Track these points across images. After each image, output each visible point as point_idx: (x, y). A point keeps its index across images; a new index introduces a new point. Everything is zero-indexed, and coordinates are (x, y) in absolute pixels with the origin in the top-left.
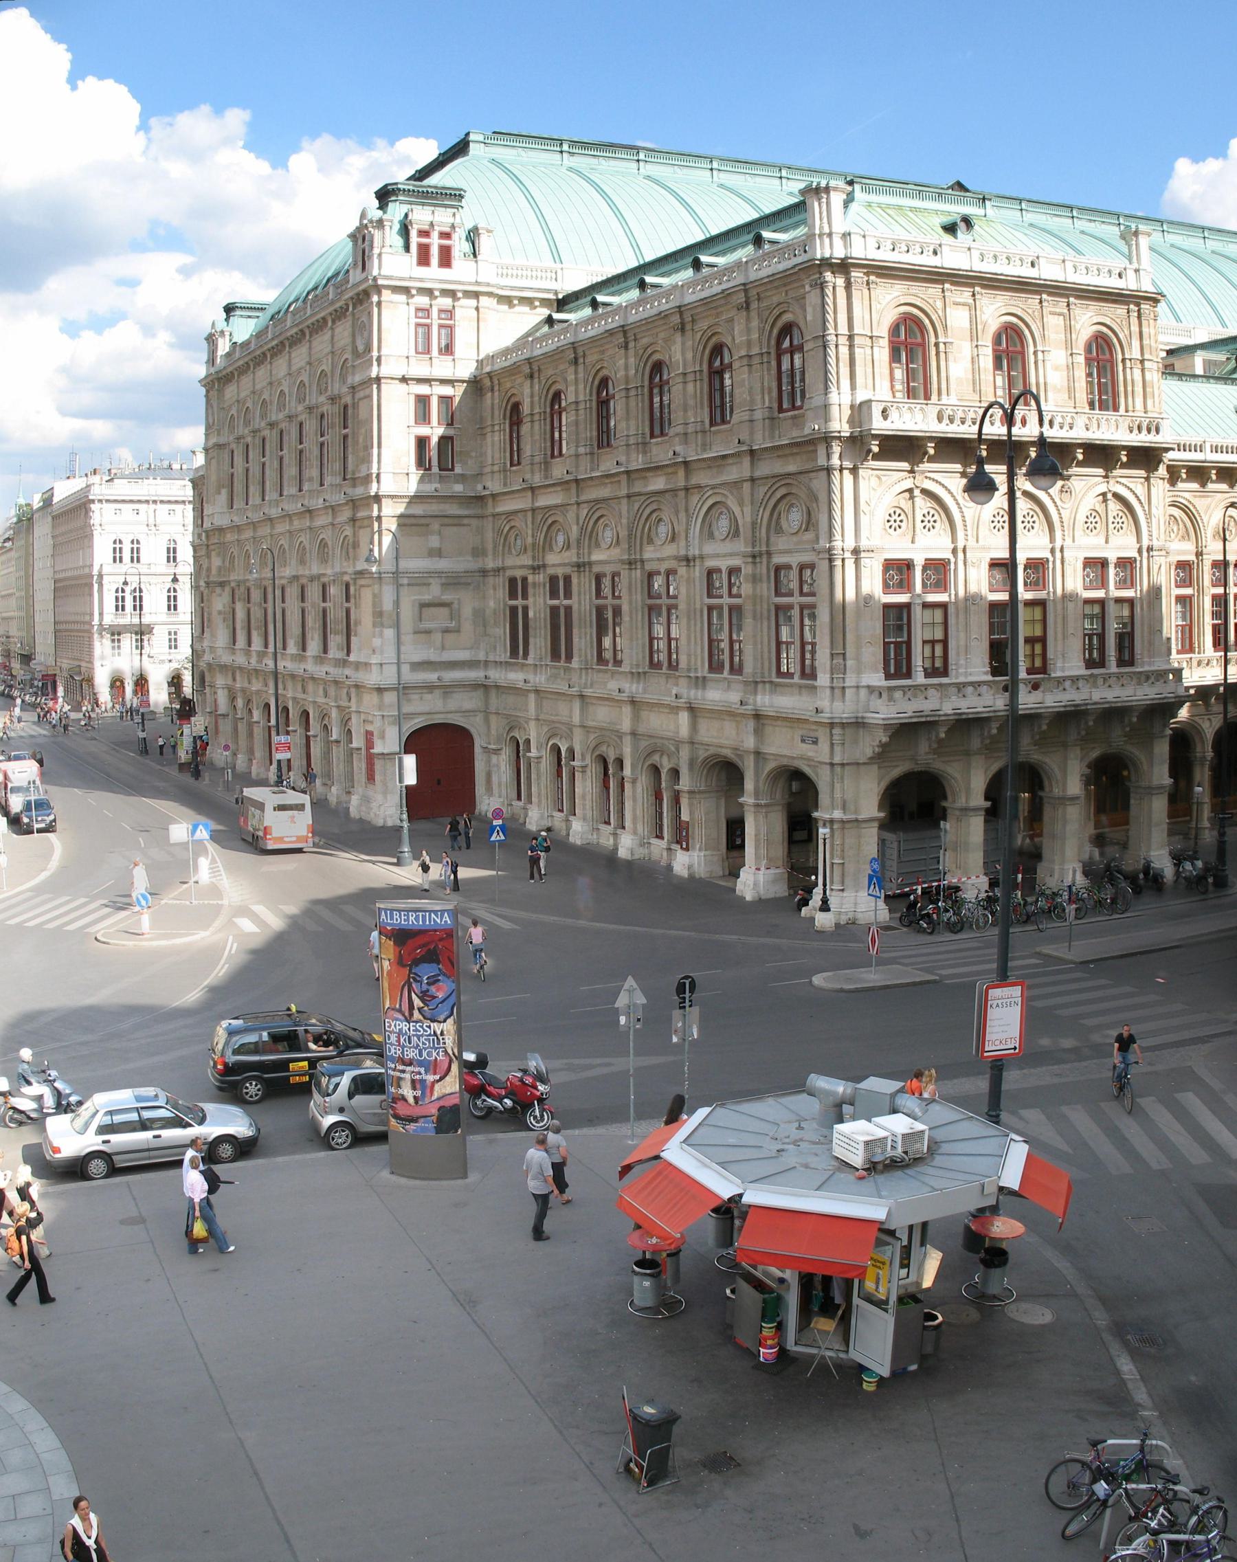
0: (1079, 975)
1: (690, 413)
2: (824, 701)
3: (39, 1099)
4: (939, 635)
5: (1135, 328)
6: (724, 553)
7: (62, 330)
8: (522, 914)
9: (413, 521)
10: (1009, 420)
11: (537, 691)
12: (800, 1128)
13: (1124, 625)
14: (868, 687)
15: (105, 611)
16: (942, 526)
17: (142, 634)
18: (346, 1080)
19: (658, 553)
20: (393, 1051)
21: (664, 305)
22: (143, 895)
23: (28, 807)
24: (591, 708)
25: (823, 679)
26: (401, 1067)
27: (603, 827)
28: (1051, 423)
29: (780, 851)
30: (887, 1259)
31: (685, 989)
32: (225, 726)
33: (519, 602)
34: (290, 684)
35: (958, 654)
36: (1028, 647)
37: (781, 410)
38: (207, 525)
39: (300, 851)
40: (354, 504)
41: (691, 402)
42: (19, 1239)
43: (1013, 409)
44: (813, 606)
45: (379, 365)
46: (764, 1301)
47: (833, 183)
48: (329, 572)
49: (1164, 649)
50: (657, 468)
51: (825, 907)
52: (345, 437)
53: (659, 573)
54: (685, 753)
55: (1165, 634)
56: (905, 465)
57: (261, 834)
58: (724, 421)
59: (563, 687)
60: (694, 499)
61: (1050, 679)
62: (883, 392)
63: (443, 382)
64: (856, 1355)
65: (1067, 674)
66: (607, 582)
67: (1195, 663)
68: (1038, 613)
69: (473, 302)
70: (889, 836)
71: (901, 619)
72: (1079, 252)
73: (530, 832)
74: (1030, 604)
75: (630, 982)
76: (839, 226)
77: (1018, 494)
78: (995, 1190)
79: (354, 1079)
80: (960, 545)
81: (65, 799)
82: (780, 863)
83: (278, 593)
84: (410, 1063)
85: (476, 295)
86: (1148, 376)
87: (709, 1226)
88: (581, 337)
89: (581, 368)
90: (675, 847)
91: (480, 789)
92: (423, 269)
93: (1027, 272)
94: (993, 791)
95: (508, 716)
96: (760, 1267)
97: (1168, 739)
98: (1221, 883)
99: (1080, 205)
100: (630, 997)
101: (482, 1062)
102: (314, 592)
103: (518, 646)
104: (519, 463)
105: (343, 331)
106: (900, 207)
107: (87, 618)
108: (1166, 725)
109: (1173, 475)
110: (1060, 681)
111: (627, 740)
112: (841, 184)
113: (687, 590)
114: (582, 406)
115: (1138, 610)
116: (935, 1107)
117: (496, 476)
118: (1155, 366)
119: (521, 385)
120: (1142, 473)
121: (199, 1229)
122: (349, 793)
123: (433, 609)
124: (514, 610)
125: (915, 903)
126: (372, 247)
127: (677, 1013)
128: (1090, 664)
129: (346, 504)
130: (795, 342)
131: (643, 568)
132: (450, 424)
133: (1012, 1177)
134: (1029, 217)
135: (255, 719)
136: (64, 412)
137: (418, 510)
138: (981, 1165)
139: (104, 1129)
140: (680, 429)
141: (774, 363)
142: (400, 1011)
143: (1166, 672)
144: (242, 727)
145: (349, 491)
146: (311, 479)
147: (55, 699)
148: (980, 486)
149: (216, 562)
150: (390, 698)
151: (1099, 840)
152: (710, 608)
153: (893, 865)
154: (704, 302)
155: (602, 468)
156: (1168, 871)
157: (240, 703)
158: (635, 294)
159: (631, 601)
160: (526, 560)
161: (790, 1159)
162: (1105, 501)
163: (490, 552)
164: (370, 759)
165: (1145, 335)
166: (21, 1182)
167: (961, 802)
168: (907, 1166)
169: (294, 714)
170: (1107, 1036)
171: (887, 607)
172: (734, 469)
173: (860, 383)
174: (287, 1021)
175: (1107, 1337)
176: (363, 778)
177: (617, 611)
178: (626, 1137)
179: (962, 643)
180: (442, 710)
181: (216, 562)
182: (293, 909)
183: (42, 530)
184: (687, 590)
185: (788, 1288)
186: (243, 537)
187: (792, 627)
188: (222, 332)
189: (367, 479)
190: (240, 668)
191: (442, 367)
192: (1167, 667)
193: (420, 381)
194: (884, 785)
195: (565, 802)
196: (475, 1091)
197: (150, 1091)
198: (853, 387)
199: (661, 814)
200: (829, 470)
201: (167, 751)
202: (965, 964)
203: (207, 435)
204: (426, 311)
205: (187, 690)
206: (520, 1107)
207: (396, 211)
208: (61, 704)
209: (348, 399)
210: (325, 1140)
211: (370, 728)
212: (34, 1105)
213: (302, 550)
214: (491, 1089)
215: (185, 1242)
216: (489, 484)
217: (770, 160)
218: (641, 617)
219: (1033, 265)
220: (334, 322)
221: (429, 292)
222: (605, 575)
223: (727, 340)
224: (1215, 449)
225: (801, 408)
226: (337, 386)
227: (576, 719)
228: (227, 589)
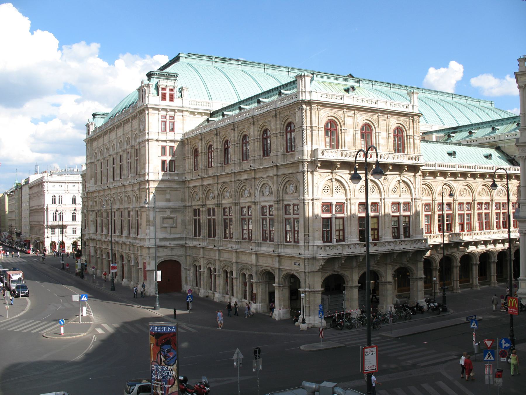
1: (256, 153)
4: (341, 228)
5: (411, 125)
6: (267, 201)
7: (31, 122)
9: (161, 189)
10: (366, 155)
11: (203, 248)
13: (406, 224)
14: (317, 246)
15: (49, 220)
16: (342, 191)
17: (63, 229)
18: (136, 388)
19: (245, 200)
21: (247, 115)
23: (18, 287)
25: (301, 243)
26: (157, 383)
27: (226, 296)
28: (381, 157)
29: (287, 303)
31: (257, 352)
32: (93, 260)
33: (197, 217)
34: (117, 246)
35: (348, 234)
36: (372, 232)
37: (287, 152)
38: (87, 190)
40: (140, 183)
41: (256, 149)
43: (367, 152)
44: (298, 218)
45: (148, 135)
47: (306, 74)
48: (131, 207)
49: (421, 232)
50: (245, 171)
51: (304, 322)
52: (137, 160)
53: (245, 207)
54: (254, 269)
55: (421, 227)
56: (330, 171)
58: (267, 156)
59: (213, 247)
60: (258, 182)
61: (380, 242)
62: (322, 146)
63: (171, 141)
65: (386, 240)
66: (227, 210)
67: (432, 237)
68: (376, 220)
69: (181, 114)
70: (325, 297)
72: (392, 99)
74: (372, 217)
75: (238, 350)
76: (308, 89)
77: (369, 181)
79: (140, 387)
80: (348, 198)
81: (33, 285)
83: (113, 214)
84: (160, 381)
85: (182, 111)
86: (415, 141)
88: (219, 126)
89: (219, 137)
91: (183, 283)
92: (164, 102)
93: (373, 106)
94: (362, 280)
95: (193, 257)
97: (423, 263)
98: (445, 310)
99: (394, 83)
100: (238, 355)
101: (185, 380)
102: (125, 214)
103: (197, 233)
104: (197, 170)
105: (135, 123)
106: (330, 83)
107: (42, 223)
108: (422, 257)
109: (424, 174)
110: (384, 243)
111: (234, 265)
112: (309, 74)
113: (255, 213)
114: (219, 150)
115: (411, 219)
117: (189, 174)
118: (418, 138)
119: (198, 143)
120: (413, 174)
124: (195, 220)
126: (145, 94)
127: (254, 361)
128: (394, 237)
129: (137, 183)
130: (292, 129)
132: (173, 156)
134: (375, 87)
135: (132, 264)
136: (33, 151)
137: (162, 185)
140: (252, 158)
141: (285, 136)
142: (157, 362)
143: (422, 240)
145: (138, 179)
147: (29, 248)
148: (355, 178)
149: (90, 203)
150: (152, 251)
152: (263, 219)
154: (261, 114)
155: (226, 171)
156: (425, 305)
157: (98, 252)
158: (237, 111)
159: (235, 217)
162: (399, 183)
163: (187, 200)
164: (145, 272)
165: (415, 128)
167: (350, 284)
169: (118, 256)
171: (323, 218)
172: (271, 172)
173: (314, 143)
177: (231, 220)
179: (349, 230)
180: (170, 254)
181: (90, 203)
182: (116, 325)
183: (25, 191)
184: (255, 213)
187: (291, 226)
188: (92, 123)
189: (144, 175)
191: (170, 136)
192: (422, 238)
193: (163, 141)
194: (323, 279)
195: (213, 287)
198: (312, 144)
199: (246, 291)
200: (303, 172)
203: (87, 159)
204: (165, 117)
205: (79, 248)
207: (154, 81)
209: (137, 147)
211: (145, 261)
213: (121, 199)
214: (189, 390)
216: (187, 177)
217: (285, 66)
219: (376, 103)
220: (132, 120)
221: (166, 110)
222: (227, 208)
223: (269, 128)
224: (460, 167)
225: (294, 151)
226: (133, 142)
227: (217, 258)
228: (94, 213)
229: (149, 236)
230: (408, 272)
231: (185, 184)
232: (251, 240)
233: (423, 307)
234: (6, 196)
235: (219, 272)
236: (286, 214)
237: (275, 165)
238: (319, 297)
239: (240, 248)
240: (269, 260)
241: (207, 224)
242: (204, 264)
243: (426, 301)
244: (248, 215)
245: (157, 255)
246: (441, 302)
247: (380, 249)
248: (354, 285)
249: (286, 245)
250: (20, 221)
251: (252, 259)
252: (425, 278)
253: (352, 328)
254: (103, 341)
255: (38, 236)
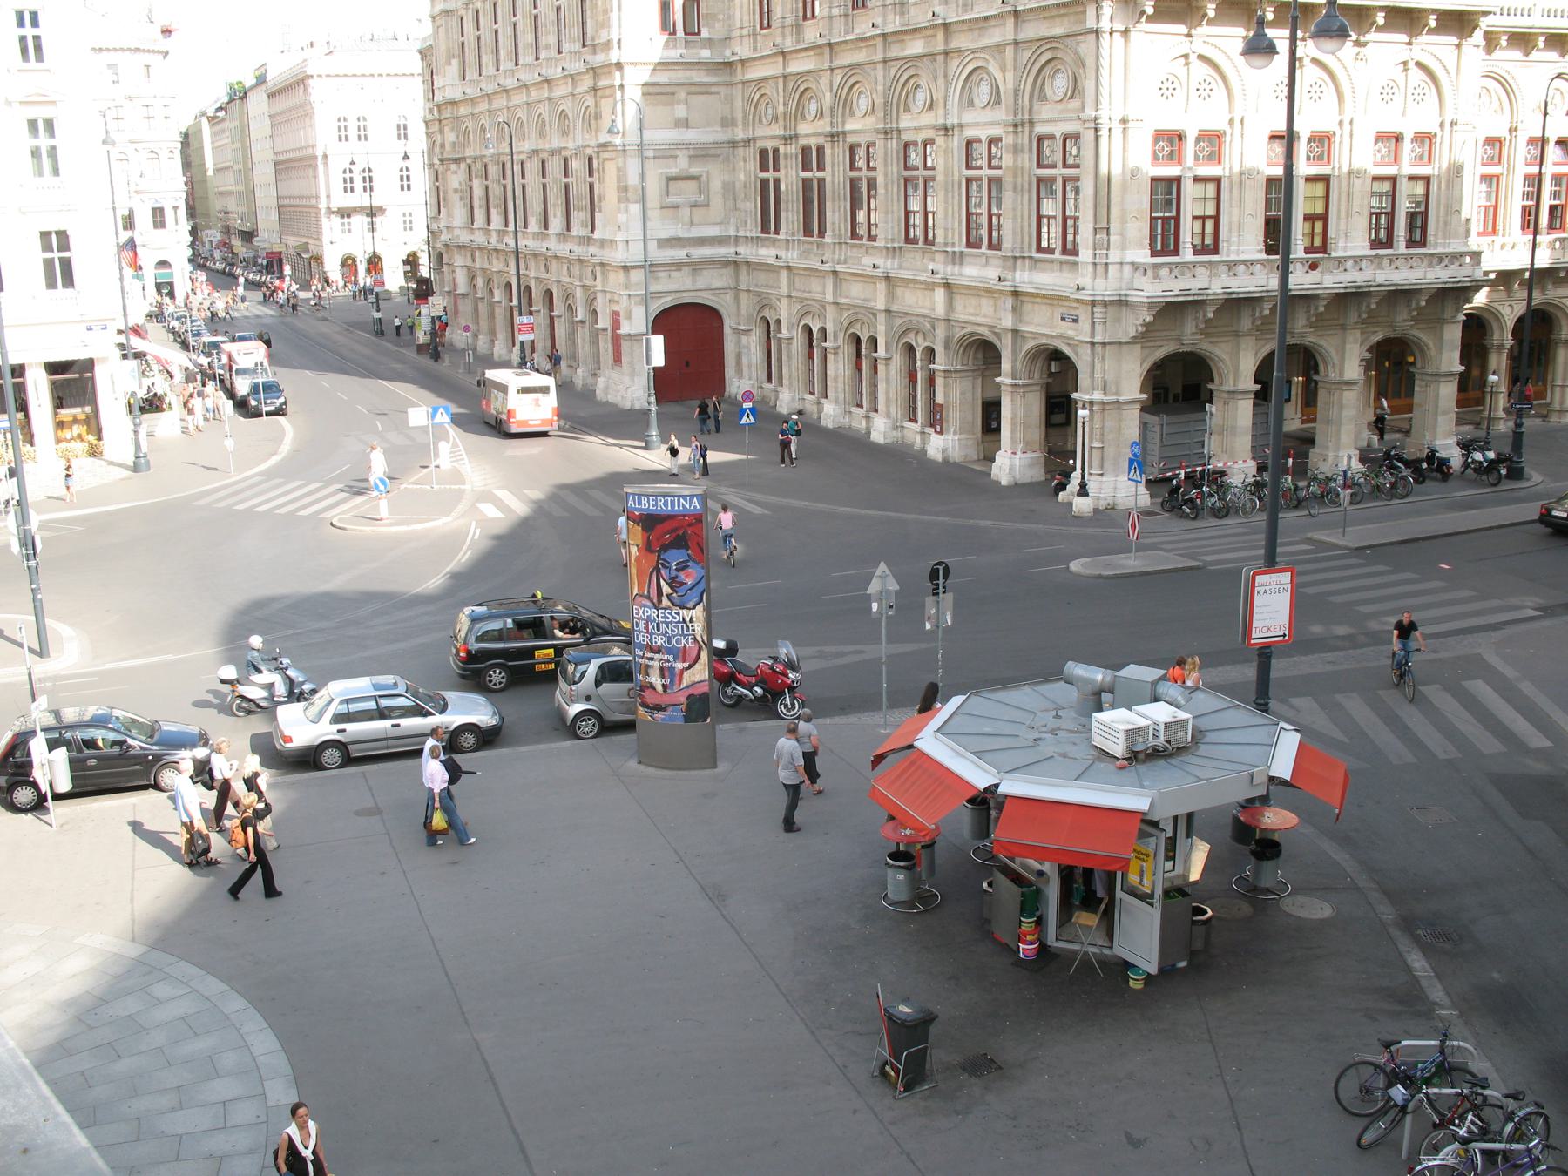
0: (1354, 561)
2: (1085, 278)
3: (270, 687)
6: (984, 122)
8: (773, 499)
9: (658, 89)
11: (788, 268)
12: (1057, 716)
13: (1418, 204)
14: (1133, 264)
18: (592, 668)
20: (641, 638)
22: (382, 481)
23: (255, 389)
24: (845, 285)
25: (1085, 255)
27: (855, 410)
29: (1037, 433)
30: (1150, 850)
31: (938, 575)
32: (465, 307)
33: (770, 175)
34: (532, 264)
35: (1230, 230)
38: (438, 98)
39: (544, 434)
40: (594, 71)
42: (245, 831)
44: (1077, 179)
46: (1023, 895)
48: (570, 145)
49: (1462, 230)
50: (915, 30)
51: (1083, 491)
54: (940, 333)
55: (1464, 216)
56: (1182, 29)
57: (504, 417)
59: (818, 265)
60: (955, 63)
61: (1330, 259)
64: (1121, 950)
66: (861, 152)
68: (1320, 187)
71: (1170, 193)
73: (780, 415)
74: (1309, 179)
75: (882, 568)
78: (1265, 779)
79: (601, 667)
81: (296, 383)
82: (1037, 447)
83: (517, 168)
87: (963, 818)
90: (930, 430)
95: (758, 294)
96: (1018, 860)
98: (1516, 474)
100: (882, 582)
101: (731, 650)
102: (555, 167)
103: (769, 222)
107: (313, 202)
108: (1458, 309)
110: (1341, 261)
111: (882, 318)
113: (945, 160)
116: (1199, 696)
117: (746, 40)
120: (1454, 40)
121: (439, 820)
122: (595, 375)
123: (681, 184)
124: (764, 183)
125: (1177, 489)
127: (930, 600)
128: (1376, 244)
131: (899, 137)
133: (1283, 766)
135: (497, 298)
137: (663, 78)
138: (1248, 754)
139: (339, 718)
142: (648, 597)
143: (1462, 254)
144: (483, 308)
145: (589, 58)
146: (548, 47)
147: (282, 277)
149: (450, 137)
151: (1379, 425)
152: (969, 181)
153: (1154, 448)
155: (857, 31)
156: (1455, 457)
157: (480, 282)
159: (886, 172)
160: (778, 130)
161: (1048, 748)
163: (740, 123)
164: (617, 340)
166: (248, 772)
167: (1229, 385)
168: (1171, 755)
170: (1386, 623)
171: (1154, 180)
174: (533, 608)
175: (1395, 932)
176: (610, 361)
177: (872, 184)
178: (879, 726)
179: (1235, 219)
181: (450, 137)
182: (537, 494)
183: (258, 104)
184: (945, 160)
185: (1048, 882)
186: (477, 110)
189: (607, 45)
190: (479, 248)
194: (1147, 366)
195: (817, 383)
196: (725, 679)
197: (389, 679)
199: (915, 397)
201: (403, 332)
202: (1228, 551)
205: (424, 272)
206: (771, 696)
208: (288, 285)
210: (571, 729)
211: (616, 308)
212: (264, 694)
214: (741, 677)
215: (423, 835)
216: (737, 49)
218: (896, 190)
227: (829, 298)
228: (463, 165)
229: (627, 231)
230: (1413, 354)
231: (733, 74)
232: (932, 243)
233: (1448, 460)
234: (204, 121)
235: (837, 341)
236: (1039, 165)
237: (1009, 9)
238: (1132, 418)
239: (900, 267)
240: (986, 306)
241: (799, 195)
242: (790, 314)
243: (1458, 444)
244: (925, 167)
245: (652, 289)
246: (1507, 450)
247: (1329, 280)
248: (1241, 386)
249: (1037, 261)
250: (249, 196)
251: (933, 303)
252: (1461, 374)
253: (1226, 515)
254: (500, 539)
255: (304, 240)
